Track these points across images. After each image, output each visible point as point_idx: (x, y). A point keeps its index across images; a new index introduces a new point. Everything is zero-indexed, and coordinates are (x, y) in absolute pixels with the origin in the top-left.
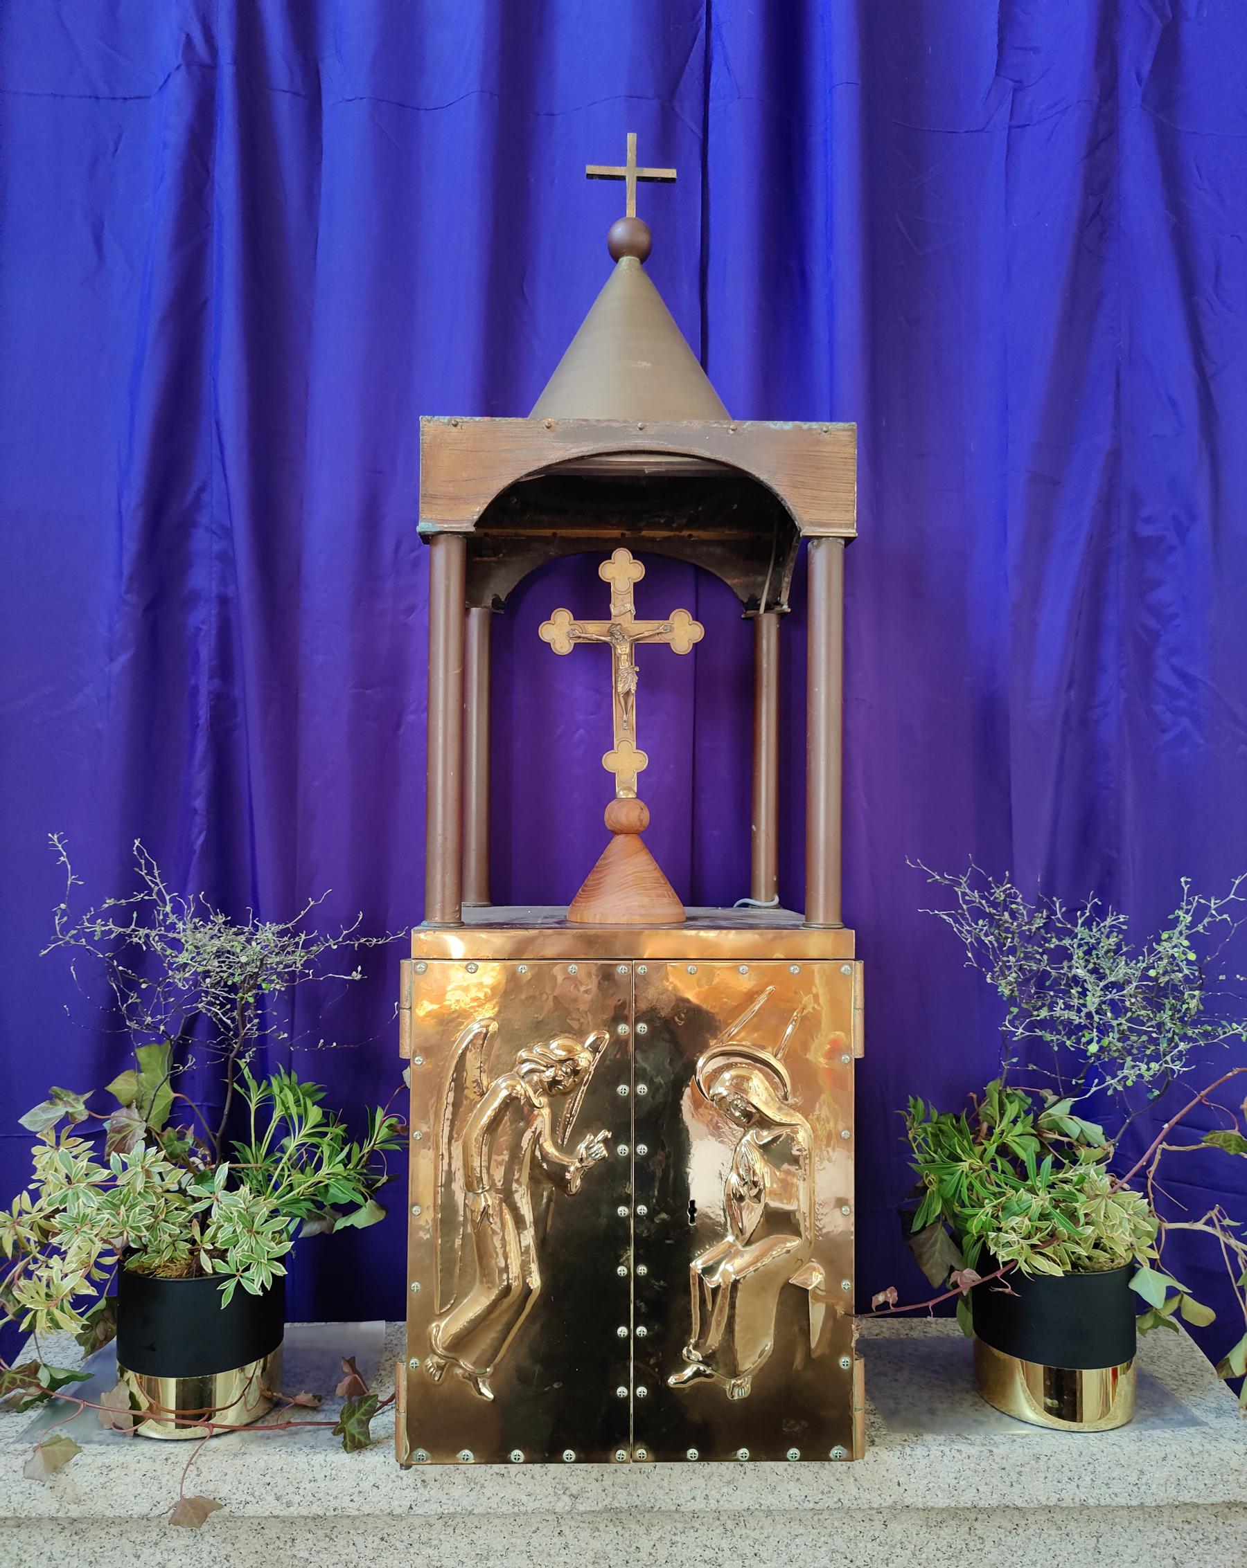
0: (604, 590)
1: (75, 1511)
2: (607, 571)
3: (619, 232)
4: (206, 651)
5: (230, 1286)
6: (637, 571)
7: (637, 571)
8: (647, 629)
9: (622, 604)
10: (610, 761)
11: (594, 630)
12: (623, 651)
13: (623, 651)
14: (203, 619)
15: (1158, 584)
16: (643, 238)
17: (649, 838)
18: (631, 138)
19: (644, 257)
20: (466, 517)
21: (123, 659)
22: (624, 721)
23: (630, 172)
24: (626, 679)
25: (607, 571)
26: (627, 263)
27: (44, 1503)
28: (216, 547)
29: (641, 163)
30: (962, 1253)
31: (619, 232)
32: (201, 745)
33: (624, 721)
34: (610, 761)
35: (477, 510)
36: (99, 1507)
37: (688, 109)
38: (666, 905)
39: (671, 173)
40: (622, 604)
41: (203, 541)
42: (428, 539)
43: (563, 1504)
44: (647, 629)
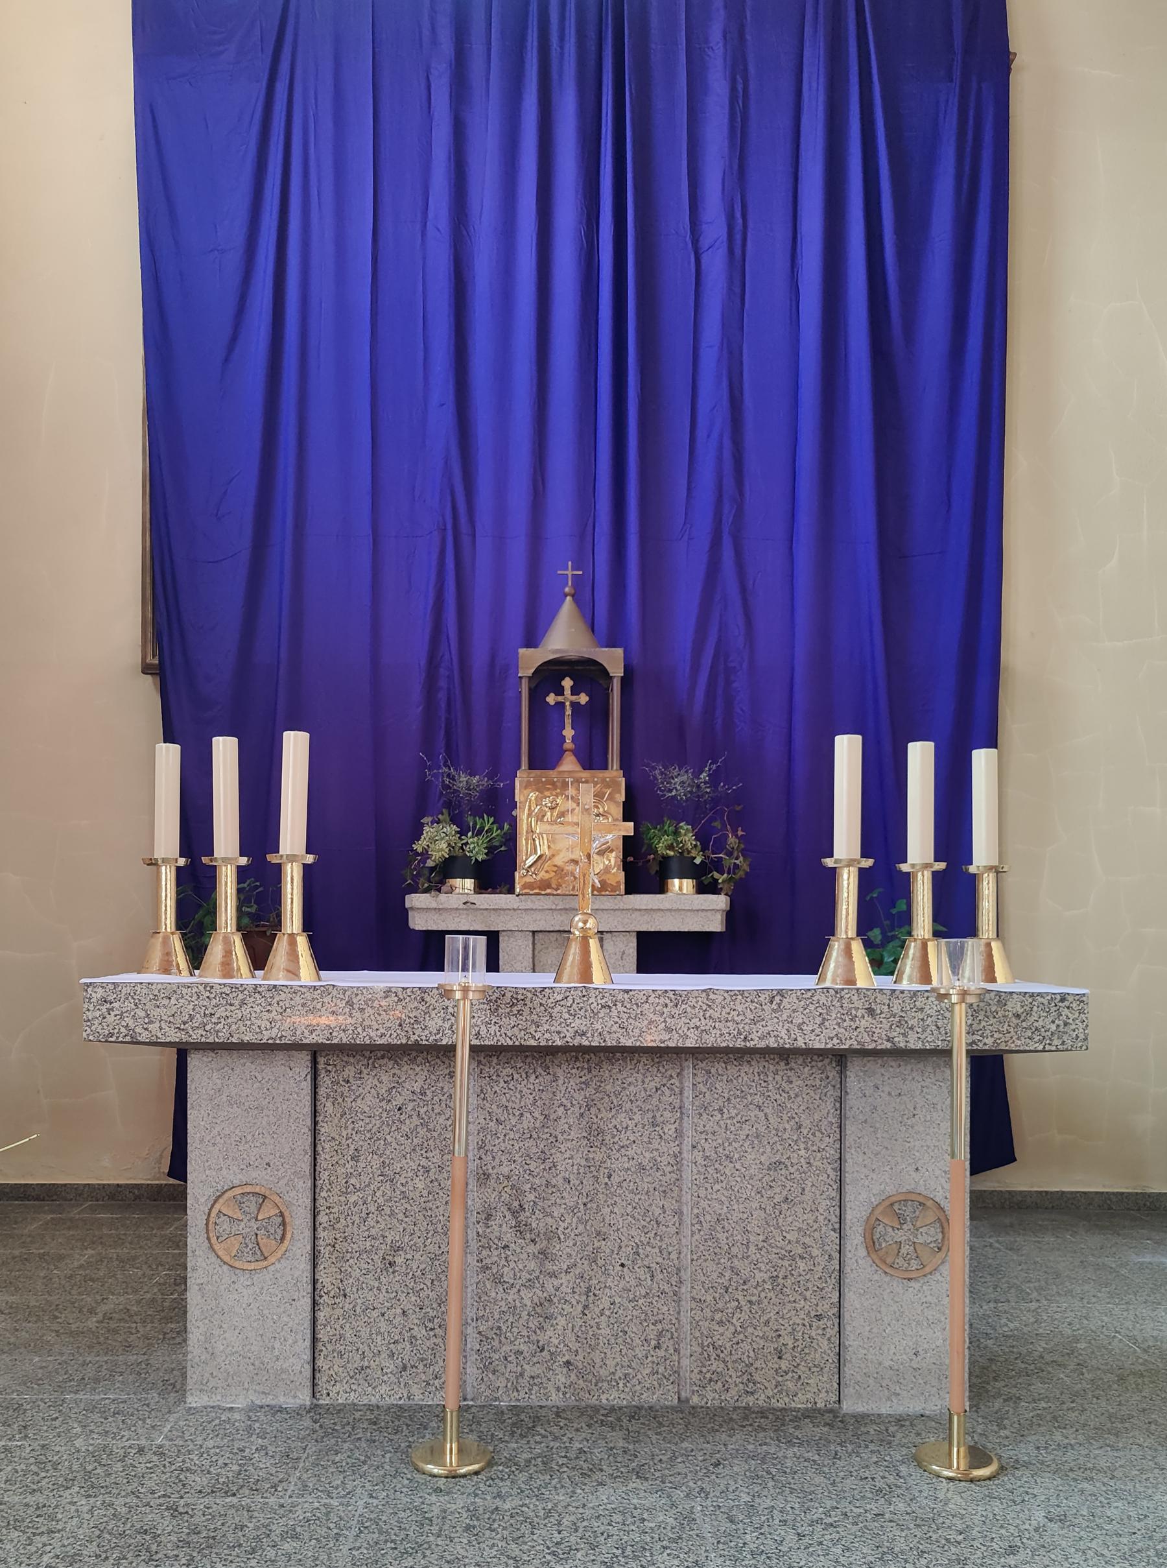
0: (557, 703)
1: (441, 907)
2: (563, 683)
3: (567, 590)
4: (443, 705)
5: (474, 859)
6: (572, 683)
7: (572, 683)
8: (574, 698)
9: (567, 692)
10: (564, 733)
11: (560, 699)
12: (568, 704)
13: (568, 704)
14: (442, 696)
15: (735, 681)
16: (573, 592)
17: (575, 753)
18: (570, 563)
19: (573, 596)
20: (530, 672)
21: (421, 708)
22: (568, 722)
23: (569, 573)
24: (568, 712)
25: (563, 683)
26: (569, 598)
27: (434, 905)
28: (447, 673)
29: (573, 570)
30: (151, 106)
31: (567, 590)
32: (442, 732)
33: (568, 722)
34: (564, 733)
35: (533, 670)
36: (446, 906)
37: (590, 528)
38: (578, 768)
39: (581, 573)
40: (567, 692)
41: (443, 671)
42: (521, 677)
43: (554, 907)
44: (574, 698)
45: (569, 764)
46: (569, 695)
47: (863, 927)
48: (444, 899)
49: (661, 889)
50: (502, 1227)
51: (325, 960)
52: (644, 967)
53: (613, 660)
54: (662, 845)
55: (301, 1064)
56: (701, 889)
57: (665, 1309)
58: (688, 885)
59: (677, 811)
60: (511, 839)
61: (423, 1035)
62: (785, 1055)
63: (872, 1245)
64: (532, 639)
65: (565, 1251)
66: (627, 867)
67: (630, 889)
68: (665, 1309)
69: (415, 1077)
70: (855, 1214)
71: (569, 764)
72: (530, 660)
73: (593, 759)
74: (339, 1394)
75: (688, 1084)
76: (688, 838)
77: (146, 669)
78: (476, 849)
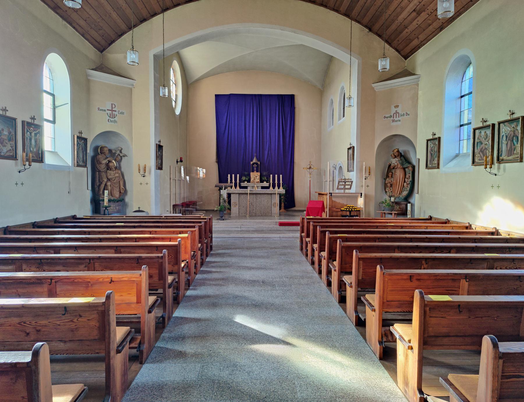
45: (255, 172)
46: (255, 166)
47: (272, 186)
48: (244, 183)
49: (263, 182)
50: (251, 205)
51: (240, 188)
52: (261, 189)
53: (259, 163)
54: (263, 179)
55: (238, 195)
56: (267, 183)
57: (261, 210)
58: (265, 182)
59: (265, 176)
60: (250, 178)
61: (246, 192)
62: (268, 194)
63: (273, 205)
64: (252, 161)
65: (254, 206)
66: (260, 180)
67: (260, 182)
68: (261, 210)
69: (245, 195)
70: (272, 204)
71: (255, 172)
72: (252, 163)
73: (257, 171)
74: (240, 215)
75: (114, 15)
76: (265, 178)
77: (216, 162)
78: (247, 179)
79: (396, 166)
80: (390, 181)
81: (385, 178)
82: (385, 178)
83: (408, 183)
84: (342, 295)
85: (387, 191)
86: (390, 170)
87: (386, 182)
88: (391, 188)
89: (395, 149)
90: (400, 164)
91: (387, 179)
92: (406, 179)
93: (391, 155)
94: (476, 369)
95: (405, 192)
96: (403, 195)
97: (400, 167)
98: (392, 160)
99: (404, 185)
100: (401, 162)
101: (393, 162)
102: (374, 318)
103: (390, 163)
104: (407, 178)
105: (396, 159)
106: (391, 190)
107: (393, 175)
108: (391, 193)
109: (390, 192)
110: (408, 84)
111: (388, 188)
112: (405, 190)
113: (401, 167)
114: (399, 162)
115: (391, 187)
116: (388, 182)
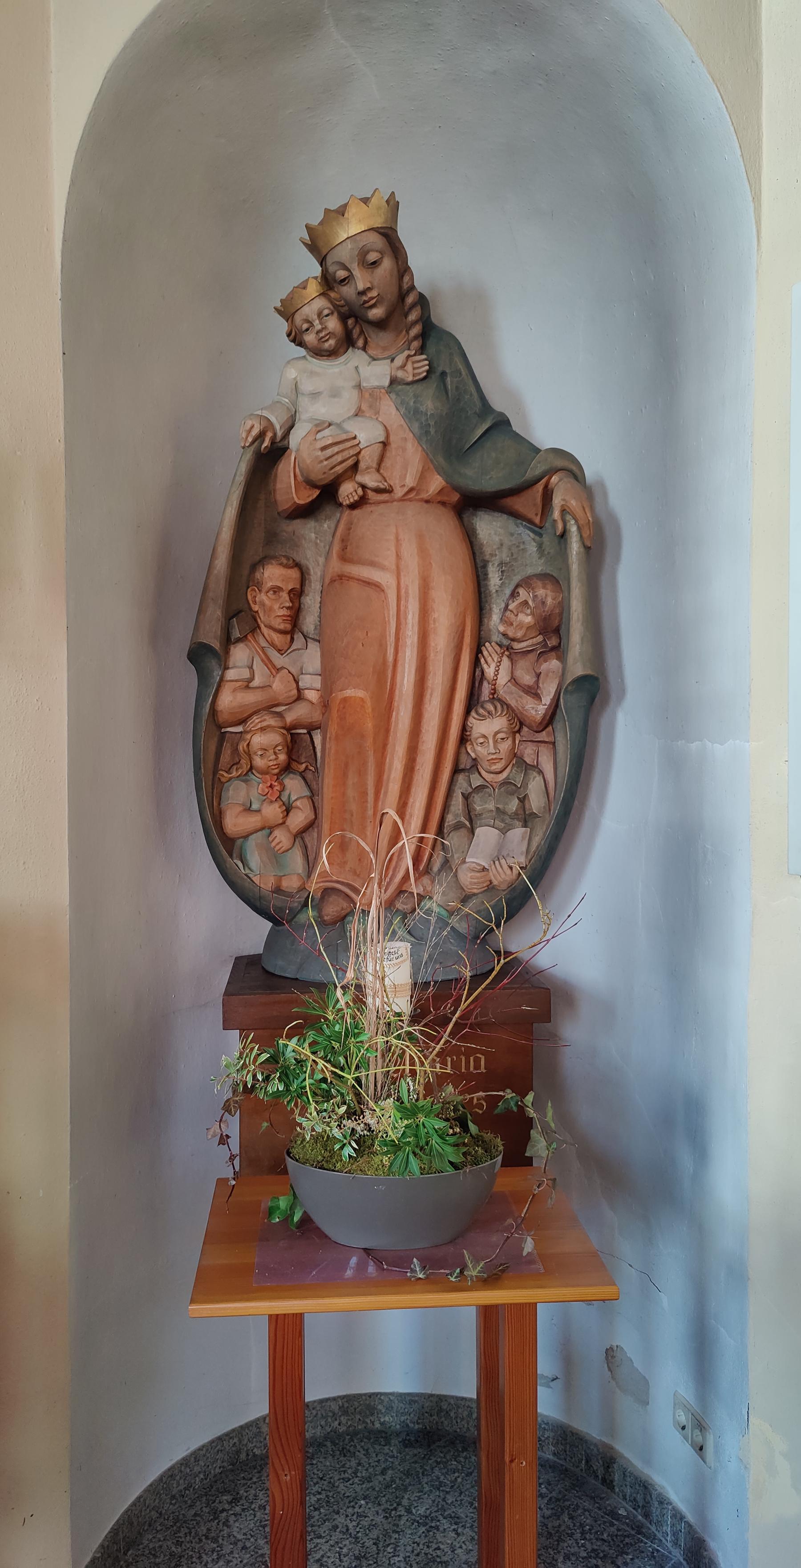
79: (368, 459)
80: (280, 686)
81: (212, 637)
82: (212, 637)
83: (537, 710)
84: (469, 743)
85: (234, 822)
86: (272, 538)
87: (228, 700)
88: (294, 786)
89: (342, 211)
90: (423, 435)
91: (240, 654)
92: (490, 652)
93: (287, 311)
94: (528, 1306)
95: (486, 835)
96: (467, 878)
97: (422, 477)
98: (292, 373)
99: (464, 738)
100: (430, 404)
101: (321, 410)
102: (402, 714)
103: (278, 423)
104: (508, 649)
105: (355, 358)
106: (298, 819)
107: (312, 601)
108: (296, 861)
109: (281, 838)
110: (391, 640)
111: (256, 788)
112: (483, 805)
113: (436, 483)
114: (412, 414)
115: (287, 769)
116: (250, 698)
